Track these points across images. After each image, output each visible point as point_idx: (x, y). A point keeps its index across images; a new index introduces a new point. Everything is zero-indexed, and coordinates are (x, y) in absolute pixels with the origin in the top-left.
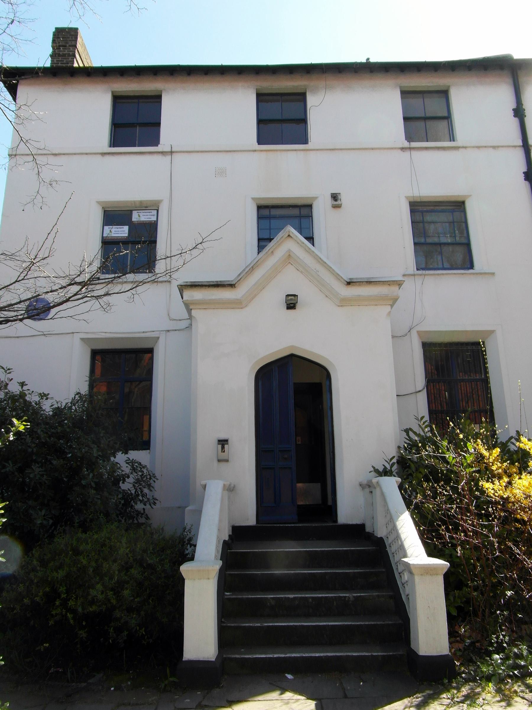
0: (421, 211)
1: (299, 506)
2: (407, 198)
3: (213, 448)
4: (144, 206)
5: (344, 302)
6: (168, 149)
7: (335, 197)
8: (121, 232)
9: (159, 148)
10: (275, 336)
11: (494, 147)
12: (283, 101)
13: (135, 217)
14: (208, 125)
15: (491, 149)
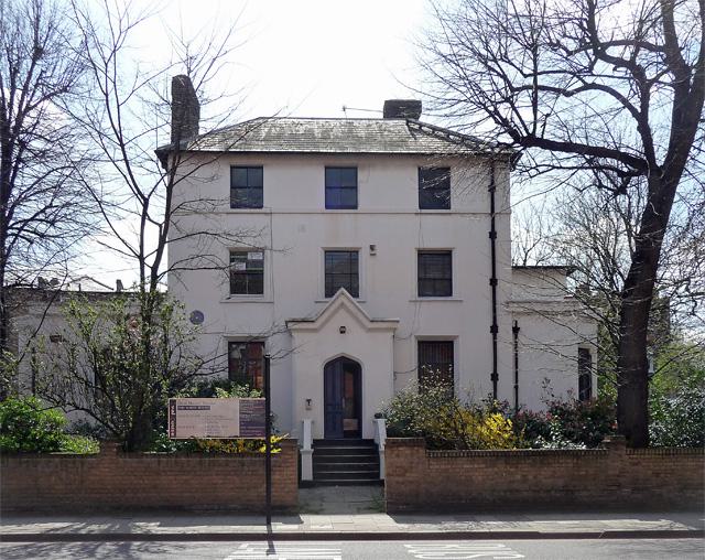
0: (425, 257)
1: (345, 432)
2: (416, 337)
3: (303, 404)
4: (257, 250)
5: (370, 330)
6: (268, 211)
7: (372, 248)
8: (242, 267)
9: (263, 210)
10: (334, 347)
11: (516, 387)
12: (342, 178)
13: (249, 257)
14: (293, 192)
15: (490, 276)
